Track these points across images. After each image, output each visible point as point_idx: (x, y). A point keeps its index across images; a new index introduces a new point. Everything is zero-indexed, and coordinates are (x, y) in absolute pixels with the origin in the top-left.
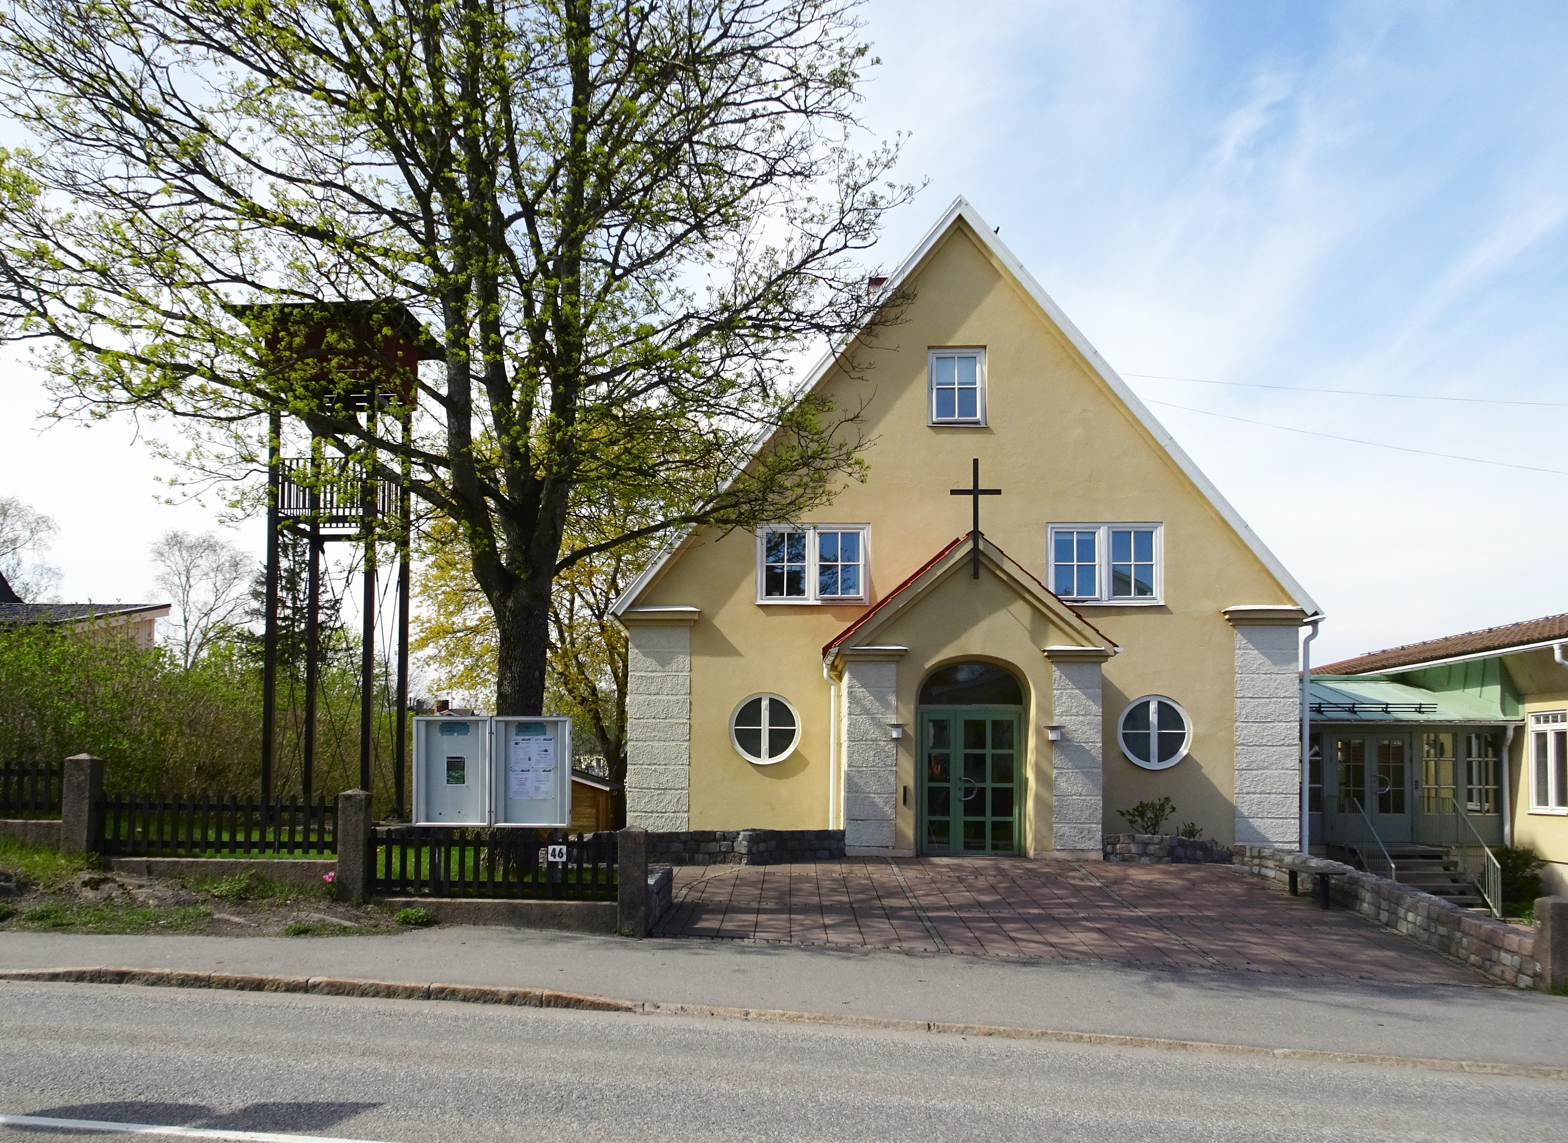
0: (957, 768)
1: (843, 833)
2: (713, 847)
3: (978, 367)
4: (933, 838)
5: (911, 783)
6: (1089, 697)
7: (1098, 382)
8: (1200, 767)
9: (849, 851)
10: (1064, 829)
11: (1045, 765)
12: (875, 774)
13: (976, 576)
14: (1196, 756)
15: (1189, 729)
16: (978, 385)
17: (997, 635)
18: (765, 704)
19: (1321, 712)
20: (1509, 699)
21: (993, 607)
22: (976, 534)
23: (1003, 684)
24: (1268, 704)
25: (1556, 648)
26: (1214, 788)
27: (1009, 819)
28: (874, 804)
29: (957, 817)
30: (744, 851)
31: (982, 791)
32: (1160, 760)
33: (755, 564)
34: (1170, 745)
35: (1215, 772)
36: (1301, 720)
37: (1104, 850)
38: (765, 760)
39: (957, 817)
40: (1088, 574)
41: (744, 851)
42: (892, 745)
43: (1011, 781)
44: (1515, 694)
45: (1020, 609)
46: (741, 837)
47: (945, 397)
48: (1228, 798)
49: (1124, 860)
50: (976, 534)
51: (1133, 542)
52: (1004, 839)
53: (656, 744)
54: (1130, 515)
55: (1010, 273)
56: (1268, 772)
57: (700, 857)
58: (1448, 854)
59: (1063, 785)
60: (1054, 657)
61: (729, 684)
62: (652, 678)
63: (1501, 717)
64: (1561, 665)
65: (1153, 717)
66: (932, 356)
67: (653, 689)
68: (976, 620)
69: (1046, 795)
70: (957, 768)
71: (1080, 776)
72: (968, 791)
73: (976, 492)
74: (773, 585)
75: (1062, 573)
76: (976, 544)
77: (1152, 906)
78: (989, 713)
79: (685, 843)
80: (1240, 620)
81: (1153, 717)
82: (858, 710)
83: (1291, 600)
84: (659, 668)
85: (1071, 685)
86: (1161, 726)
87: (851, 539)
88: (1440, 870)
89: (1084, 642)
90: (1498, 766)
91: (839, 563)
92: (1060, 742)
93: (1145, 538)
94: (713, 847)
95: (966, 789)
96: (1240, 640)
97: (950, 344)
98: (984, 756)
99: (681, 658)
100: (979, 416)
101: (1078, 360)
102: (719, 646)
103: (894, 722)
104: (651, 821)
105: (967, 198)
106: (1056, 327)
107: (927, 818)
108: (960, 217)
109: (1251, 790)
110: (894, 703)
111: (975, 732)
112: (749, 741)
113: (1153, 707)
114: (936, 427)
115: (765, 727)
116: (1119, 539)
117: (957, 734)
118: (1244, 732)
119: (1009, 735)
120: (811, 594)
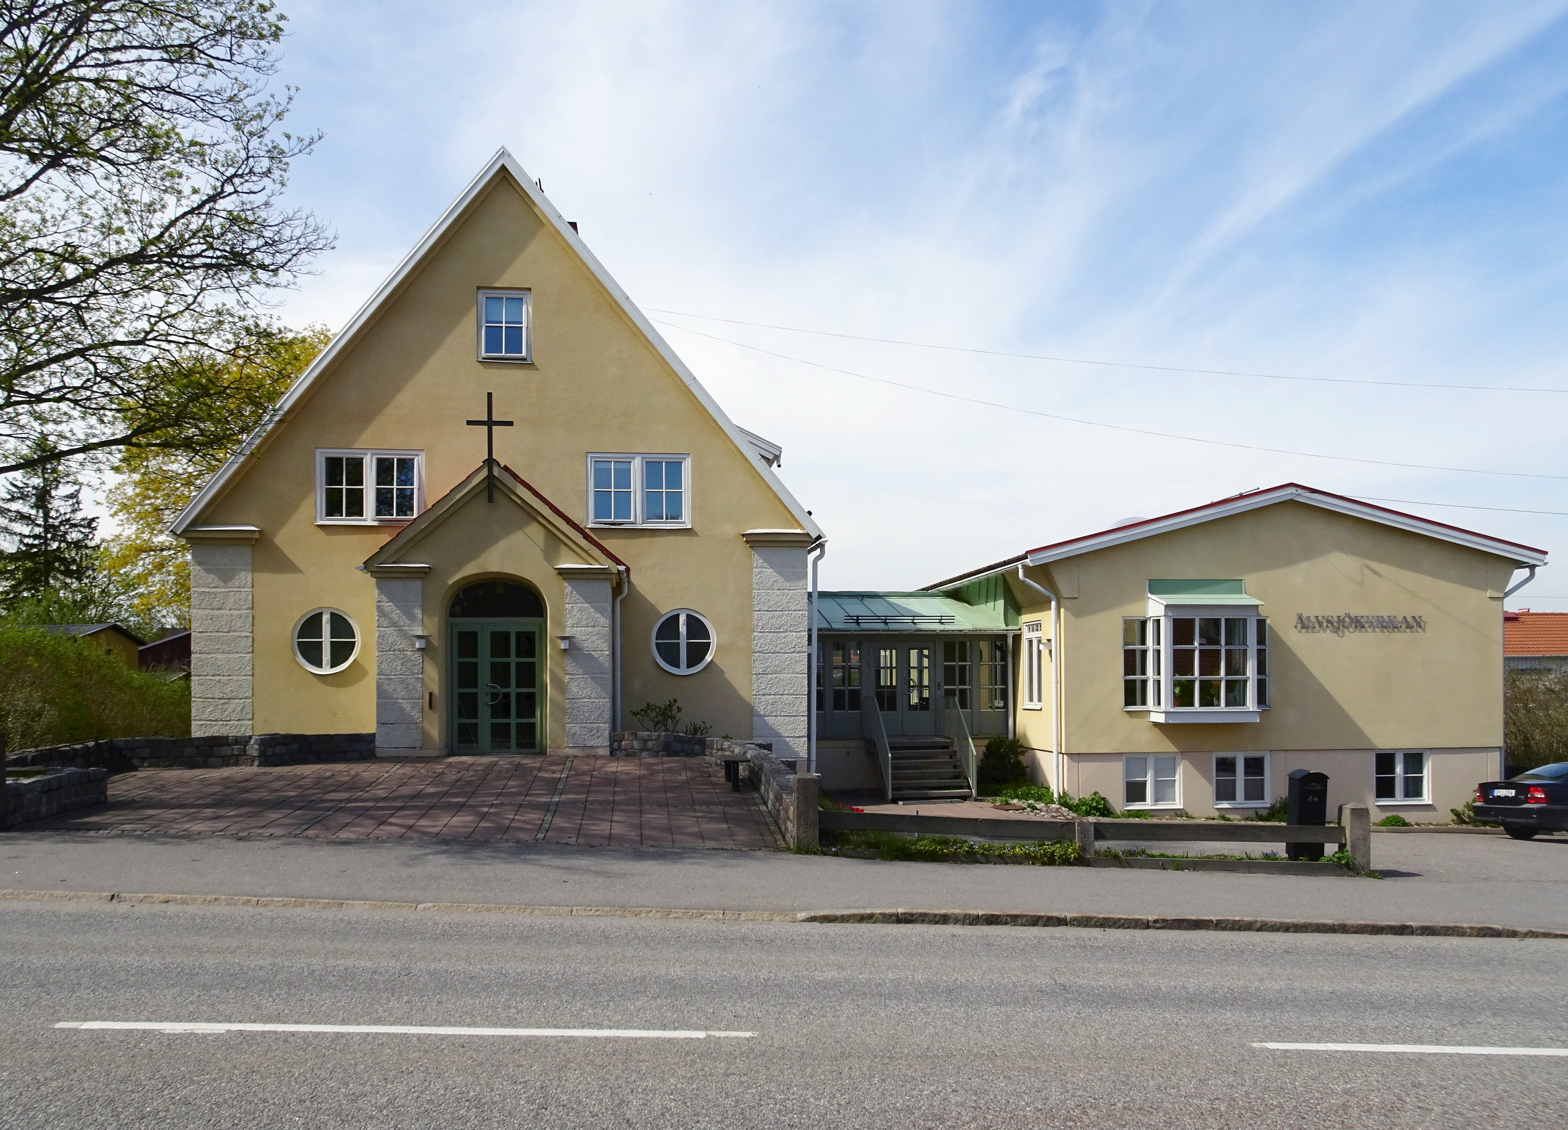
0: (484, 675)
1: (374, 735)
2: (226, 751)
3: (524, 308)
4: (462, 738)
5: (436, 689)
6: (597, 610)
7: (631, 325)
8: (723, 672)
9: (379, 752)
10: (573, 728)
11: (558, 671)
12: (402, 682)
13: (491, 500)
14: (719, 662)
15: (714, 640)
16: (524, 325)
17: (513, 554)
18: (326, 618)
19: (858, 623)
20: (1011, 611)
21: (509, 529)
22: (490, 462)
23: (518, 598)
24: (780, 616)
25: (1020, 566)
26: (734, 691)
27: (532, 720)
28: (402, 710)
29: (485, 720)
30: (255, 754)
31: (507, 696)
32: (689, 666)
33: (315, 487)
34: (697, 653)
35: (736, 677)
36: (810, 630)
37: (611, 746)
38: (326, 670)
39: (485, 720)
40: (624, 499)
41: (255, 754)
42: (418, 654)
43: (533, 686)
44: (1015, 607)
45: (534, 531)
46: (253, 741)
47: (493, 334)
48: (747, 700)
49: (628, 755)
50: (490, 462)
51: (663, 472)
52: (528, 739)
53: (220, 656)
54: (662, 446)
55: (551, 223)
56: (781, 676)
57: (213, 760)
58: (952, 744)
59: (575, 689)
60: (564, 573)
61: (288, 600)
62: (215, 594)
63: (1004, 627)
64: (1023, 582)
65: (683, 629)
66: (482, 297)
67: (216, 604)
68: (494, 539)
69: (559, 698)
70: (484, 675)
71: (590, 681)
72: (494, 696)
73: (490, 423)
74: (333, 509)
75: (602, 499)
76: (490, 471)
77: (574, 793)
78: (514, 625)
79: (198, 747)
80: (755, 542)
81: (683, 629)
82: (386, 623)
83: (800, 526)
84: (222, 584)
85: (582, 600)
86: (689, 636)
87: (406, 466)
88: (947, 759)
89: (592, 561)
90: (1004, 669)
91: (395, 487)
92: (572, 649)
93: (675, 468)
94: (226, 751)
95: (492, 694)
96: (757, 560)
97: (497, 285)
98: (509, 663)
99: (243, 574)
100: (524, 354)
101: (613, 304)
102: (281, 564)
103: (420, 633)
104: (216, 728)
105: (511, 150)
106: (593, 274)
107: (457, 721)
108: (503, 167)
109: (767, 691)
110: (420, 616)
111: (500, 641)
112: (312, 654)
113: (682, 619)
114: (486, 362)
115: (326, 639)
116: (652, 468)
117: (485, 645)
118: (761, 640)
119: (530, 644)
120: (369, 516)
